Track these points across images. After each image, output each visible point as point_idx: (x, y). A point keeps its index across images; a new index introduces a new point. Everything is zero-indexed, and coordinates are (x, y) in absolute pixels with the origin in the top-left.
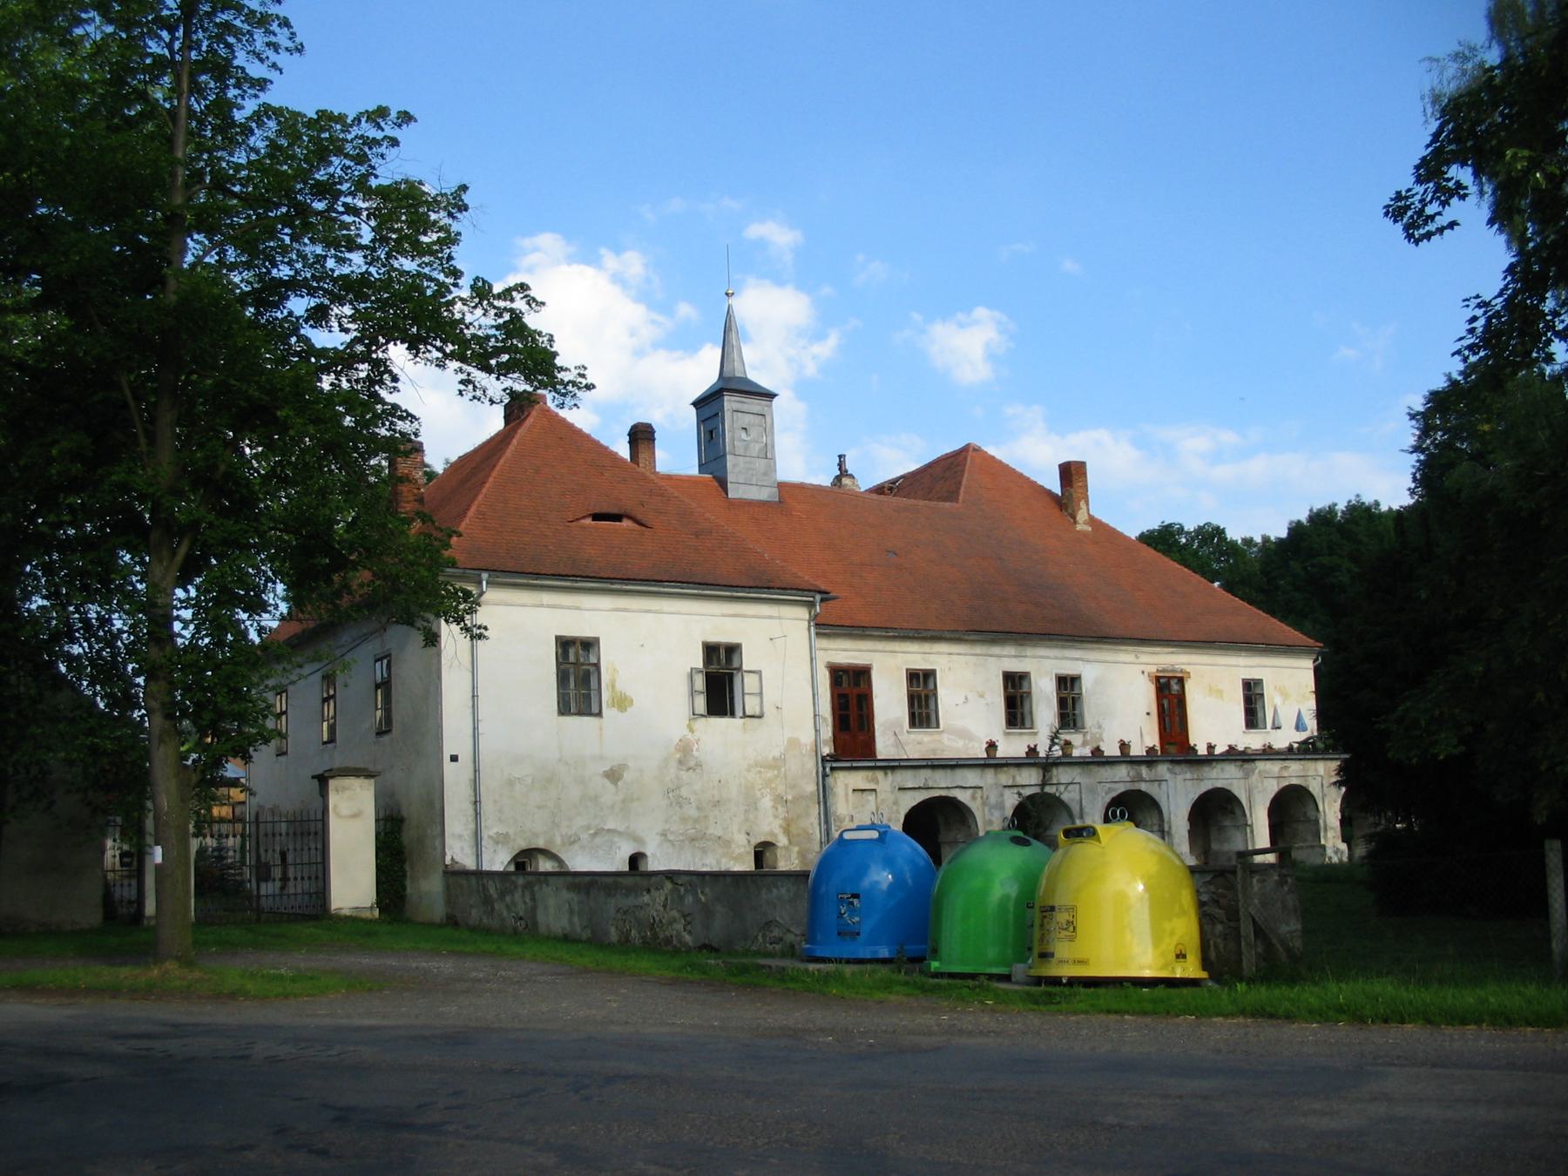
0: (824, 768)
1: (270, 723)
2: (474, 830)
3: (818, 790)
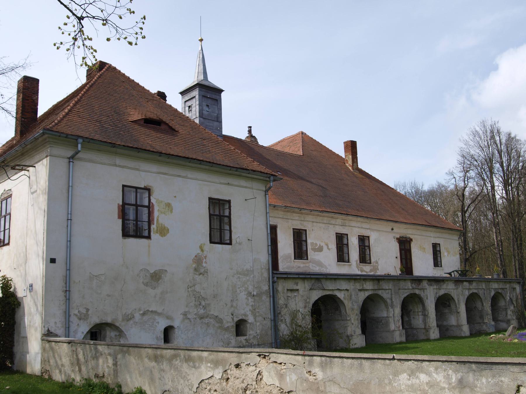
0: (273, 278)
3: (270, 288)
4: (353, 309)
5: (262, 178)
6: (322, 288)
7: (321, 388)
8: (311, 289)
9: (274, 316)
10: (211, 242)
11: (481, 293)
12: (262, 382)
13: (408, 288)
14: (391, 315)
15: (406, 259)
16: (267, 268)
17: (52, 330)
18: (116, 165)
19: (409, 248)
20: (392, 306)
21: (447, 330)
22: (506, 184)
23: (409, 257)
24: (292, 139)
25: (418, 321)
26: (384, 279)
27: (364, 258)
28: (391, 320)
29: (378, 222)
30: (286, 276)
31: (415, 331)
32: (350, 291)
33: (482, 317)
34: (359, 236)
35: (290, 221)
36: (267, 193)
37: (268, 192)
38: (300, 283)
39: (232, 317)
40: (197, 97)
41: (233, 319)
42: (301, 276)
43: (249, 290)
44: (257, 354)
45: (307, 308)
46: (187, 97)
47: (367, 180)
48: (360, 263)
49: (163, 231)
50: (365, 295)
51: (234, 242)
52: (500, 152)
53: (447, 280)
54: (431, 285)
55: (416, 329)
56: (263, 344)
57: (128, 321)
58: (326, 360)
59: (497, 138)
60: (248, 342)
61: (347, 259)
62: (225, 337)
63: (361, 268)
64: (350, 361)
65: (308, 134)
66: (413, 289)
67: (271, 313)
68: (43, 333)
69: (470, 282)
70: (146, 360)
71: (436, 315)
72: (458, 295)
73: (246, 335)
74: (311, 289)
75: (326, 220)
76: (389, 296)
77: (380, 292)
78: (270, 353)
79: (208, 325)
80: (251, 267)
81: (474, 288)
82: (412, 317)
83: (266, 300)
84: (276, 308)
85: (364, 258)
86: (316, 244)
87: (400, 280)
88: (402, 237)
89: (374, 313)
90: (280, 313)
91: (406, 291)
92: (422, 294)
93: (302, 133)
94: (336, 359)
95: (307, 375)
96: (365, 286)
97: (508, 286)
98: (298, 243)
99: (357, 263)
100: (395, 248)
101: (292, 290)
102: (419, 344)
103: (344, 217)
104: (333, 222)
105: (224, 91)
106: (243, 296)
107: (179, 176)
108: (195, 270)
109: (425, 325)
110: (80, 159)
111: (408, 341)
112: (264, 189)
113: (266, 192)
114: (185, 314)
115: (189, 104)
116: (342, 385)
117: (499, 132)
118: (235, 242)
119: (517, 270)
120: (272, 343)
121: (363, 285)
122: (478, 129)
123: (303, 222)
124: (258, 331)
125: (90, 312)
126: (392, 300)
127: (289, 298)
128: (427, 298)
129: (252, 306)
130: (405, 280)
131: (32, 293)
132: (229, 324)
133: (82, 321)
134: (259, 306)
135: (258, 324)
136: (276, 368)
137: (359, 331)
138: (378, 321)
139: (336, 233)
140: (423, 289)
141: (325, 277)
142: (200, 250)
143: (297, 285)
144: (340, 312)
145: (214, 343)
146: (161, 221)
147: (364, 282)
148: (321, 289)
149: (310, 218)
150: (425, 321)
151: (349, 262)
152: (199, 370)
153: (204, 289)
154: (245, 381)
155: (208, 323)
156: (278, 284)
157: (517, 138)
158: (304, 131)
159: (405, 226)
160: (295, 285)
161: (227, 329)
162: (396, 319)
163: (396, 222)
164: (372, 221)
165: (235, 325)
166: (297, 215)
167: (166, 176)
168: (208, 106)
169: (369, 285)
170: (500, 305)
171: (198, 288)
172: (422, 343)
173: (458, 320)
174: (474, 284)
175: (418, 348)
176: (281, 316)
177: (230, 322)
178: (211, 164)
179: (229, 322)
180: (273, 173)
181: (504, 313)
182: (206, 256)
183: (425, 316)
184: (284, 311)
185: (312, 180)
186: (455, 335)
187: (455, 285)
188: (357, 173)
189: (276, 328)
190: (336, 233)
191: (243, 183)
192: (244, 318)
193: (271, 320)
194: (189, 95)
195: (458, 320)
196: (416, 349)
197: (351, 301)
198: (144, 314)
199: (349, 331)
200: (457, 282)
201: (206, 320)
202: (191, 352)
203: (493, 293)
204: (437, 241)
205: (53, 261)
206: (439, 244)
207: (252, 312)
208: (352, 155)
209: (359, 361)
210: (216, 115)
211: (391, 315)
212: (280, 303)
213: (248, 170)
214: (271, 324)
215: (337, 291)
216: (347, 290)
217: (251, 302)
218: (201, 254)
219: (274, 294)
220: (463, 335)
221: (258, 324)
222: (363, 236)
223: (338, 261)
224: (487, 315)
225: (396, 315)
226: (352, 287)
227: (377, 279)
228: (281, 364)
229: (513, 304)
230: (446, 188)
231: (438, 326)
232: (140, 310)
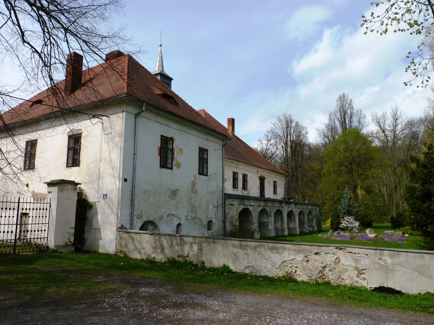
0: (225, 197)
1: (390, 144)
2: (130, 212)
3: (222, 203)
4: (255, 217)
5: (221, 137)
7: (390, 268)
10: (199, 174)
12: (340, 263)
14: (270, 221)
17: (124, 225)
18: (158, 122)
27: (244, 187)
28: (270, 224)
29: (252, 167)
44: (335, 247)
47: (239, 142)
49: (179, 165)
51: (208, 174)
53: (292, 203)
57: (160, 220)
64: (413, 254)
68: (119, 227)
70: (231, 247)
72: (296, 211)
73: (211, 230)
74: (239, 204)
77: (266, 208)
78: (346, 247)
81: (292, 207)
85: (244, 187)
91: (276, 208)
92: (282, 210)
93: (203, 110)
94: (402, 253)
95: (379, 261)
97: (314, 208)
100: (258, 182)
103: (237, 162)
104: (232, 165)
106: (211, 206)
107: (187, 133)
108: (192, 190)
109: (282, 227)
110: (141, 116)
114: (186, 216)
116: (407, 267)
125: (143, 214)
131: (106, 200)
133: (138, 219)
136: (352, 256)
139: (233, 172)
140: (283, 207)
144: (248, 218)
146: (177, 159)
150: (282, 225)
151: (237, 189)
152: (282, 255)
154: (323, 263)
158: (204, 109)
161: (204, 226)
163: (260, 168)
164: (250, 166)
167: (181, 132)
171: (192, 201)
173: (294, 225)
174: (302, 205)
179: (205, 223)
183: (282, 222)
190: (233, 172)
192: (211, 220)
195: (294, 225)
198: (168, 216)
201: (195, 221)
202: (247, 242)
204: (276, 180)
205: (126, 180)
209: (421, 254)
211: (270, 221)
216: (253, 206)
224: (306, 223)
225: (272, 221)
226: (256, 204)
228: (355, 253)
232: (166, 213)
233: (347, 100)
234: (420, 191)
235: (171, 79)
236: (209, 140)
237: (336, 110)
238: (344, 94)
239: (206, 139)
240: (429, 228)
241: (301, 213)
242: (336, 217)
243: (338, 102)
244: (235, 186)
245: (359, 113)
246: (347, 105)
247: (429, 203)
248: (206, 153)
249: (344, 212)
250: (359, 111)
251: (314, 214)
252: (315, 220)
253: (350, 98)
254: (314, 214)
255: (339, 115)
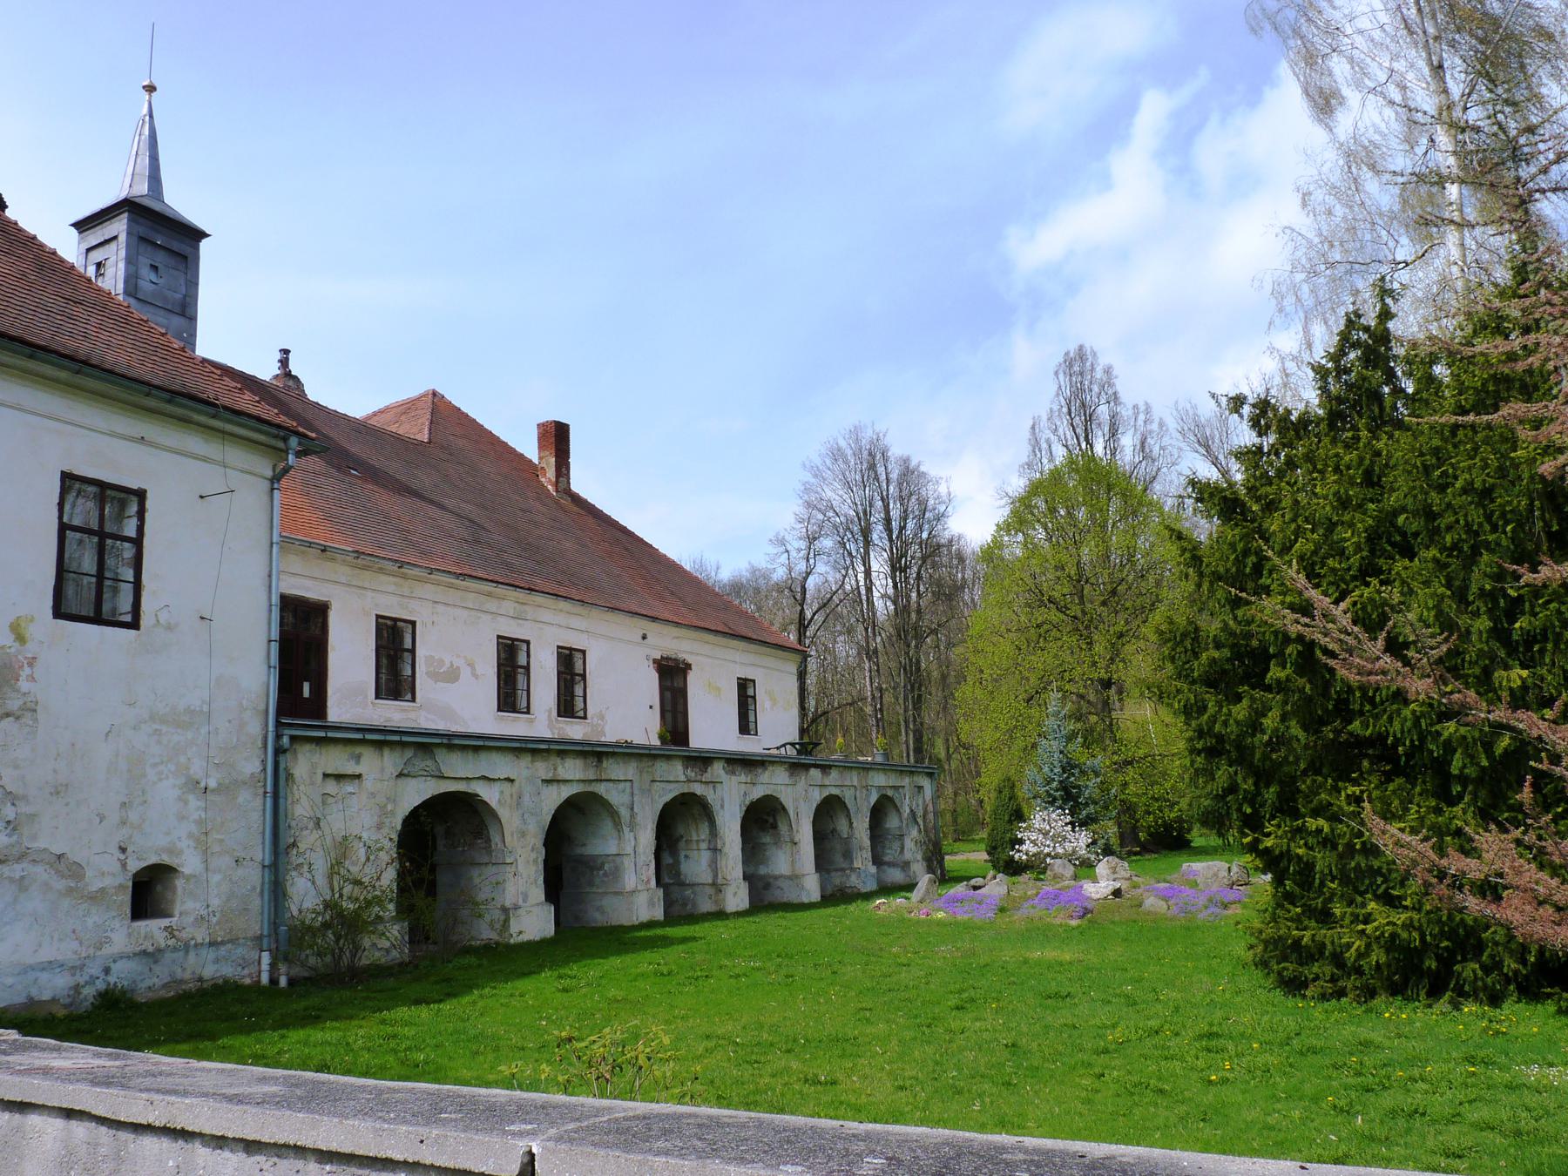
0: (278, 737)
3: (264, 770)
5: (262, 438)
6: (438, 773)
8: (400, 775)
9: (276, 851)
10: (59, 613)
11: (848, 796)
13: (674, 779)
14: (629, 850)
15: (674, 711)
16: (262, 707)
19: (681, 685)
20: (633, 826)
21: (767, 886)
22: (897, 566)
23: (680, 708)
24: (407, 408)
25: (696, 866)
26: (614, 754)
28: (628, 863)
29: (610, 616)
30: (322, 734)
31: (688, 892)
32: (517, 784)
33: (848, 855)
34: (558, 647)
35: (370, 594)
36: (276, 486)
37: (279, 480)
38: (369, 755)
39: (122, 857)
40: (123, 238)
41: (124, 865)
42: (369, 737)
43: (192, 772)
45: (385, 831)
46: (95, 237)
47: (590, 520)
48: (559, 715)
50: (559, 794)
51: (146, 620)
52: (885, 501)
54: (733, 773)
55: (692, 885)
56: (230, 941)
58: (94, 1145)
59: (881, 470)
60: (174, 937)
61: (524, 704)
62: (90, 922)
63: (560, 728)
65: (448, 397)
66: (689, 781)
67: (263, 843)
69: (825, 768)
71: (743, 849)
72: (796, 800)
73: (170, 916)
74: (400, 775)
75: (471, 600)
76: (626, 799)
77: (601, 789)
79: (22, 884)
80: (203, 702)
81: (834, 783)
82: (682, 854)
83: (251, 810)
84: (282, 826)
85: (567, 706)
86: (441, 662)
87: (655, 757)
88: (668, 659)
89: (584, 845)
90: (294, 845)
91: (672, 786)
93: (434, 394)
94: (149, 1143)
96: (560, 769)
97: (906, 781)
98: (389, 656)
99: (549, 716)
100: (649, 685)
101: (339, 777)
102: (697, 927)
104: (492, 605)
105: (208, 235)
106: (167, 791)
109: (715, 876)
111: (671, 918)
112: (269, 473)
113: (272, 483)
115: (97, 256)
117: (885, 458)
118: (153, 621)
119: (911, 753)
120: (260, 938)
121: (555, 769)
122: (843, 444)
123: (406, 600)
124: (215, 902)
126: (632, 809)
127: (330, 800)
128: (722, 806)
129: (199, 822)
130: (669, 758)
132: (107, 882)
134: (223, 823)
135: (216, 878)
137: (538, 893)
138: (591, 865)
139: (499, 637)
141: (445, 741)
142: (12, 637)
143: (358, 762)
144: (489, 840)
145: (40, 945)
147: (559, 761)
148: (432, 776)
149: (428, 591)
151: (528, 712)
153: (16, 767)
155: (22, 878)
156: (296, 758)
157: (922, 469)
158: (440, 390)
159: (675, 631)
160: (353, 762)
161: (98, 897)
162: (642, 859)
163: (654, 619)
164: (595, 612)
165: (130, 884)
166: (391, 579)
168: (154, 268)
169: (573, 769)
170: (887, 826)
172: (706, 925)
174: (834, 774)
175: (694, 939)
176: (299, 854)
177: (114, 875)
178: (76, 366)
180: (301, 429)
181: (896, 845)
182: (34, 658)
184: (308, 839)
185: (446, 502)
186: (785, 900)
187: (791, 775)
188: (566, 502)
189: (277, 891)
190: (499, 637)
191: (194, 442)
192: (166, 859)
193: (264, 866)
194: (99, 233)
196: (690, 944)
197: (520, 812)
199: (510, 896)
200: (795, 767)
203: (874, 798)
206: (754, 681)
207: (197, 841)
208: (556, 456)
210: (179, 296)
211: (629, 850)
212: (297, 814)
213: (215, 405)
214: (263, 876)
215: (481, 782)
217: (198, 809)
218: (13, 650)
219: (278, 786)
220: (806, 900)
221: (216, 878)
222: (571, 649)
223: (499, 710)
224: (861, 849)
225: (640, 849)
226: (525, 773)
227: (596, 753)
229: (917, 823)
230: (766, 576)
231: (746, 877)
233: (1093, 370)
234: (1218, 645)
235: (198, 235)
236: (151, 444)
237: (1055, 408)
238: (1081, 348)
239: (132, 439)
240: (1268, 835)
241: (829, 809)
242: (1007, 818)
243: (1061, 376)
244: (510, 697)
245: (1142, 417)
246: (1096, 389)
247: (1253, 699)
248: (133, 508)
249: (1049, 795)
250: (1142, 408)
251: (906, 811)
252: (914, 833)
253: (1103, 361)
254: (906, 811)
255: (1064, 428)
